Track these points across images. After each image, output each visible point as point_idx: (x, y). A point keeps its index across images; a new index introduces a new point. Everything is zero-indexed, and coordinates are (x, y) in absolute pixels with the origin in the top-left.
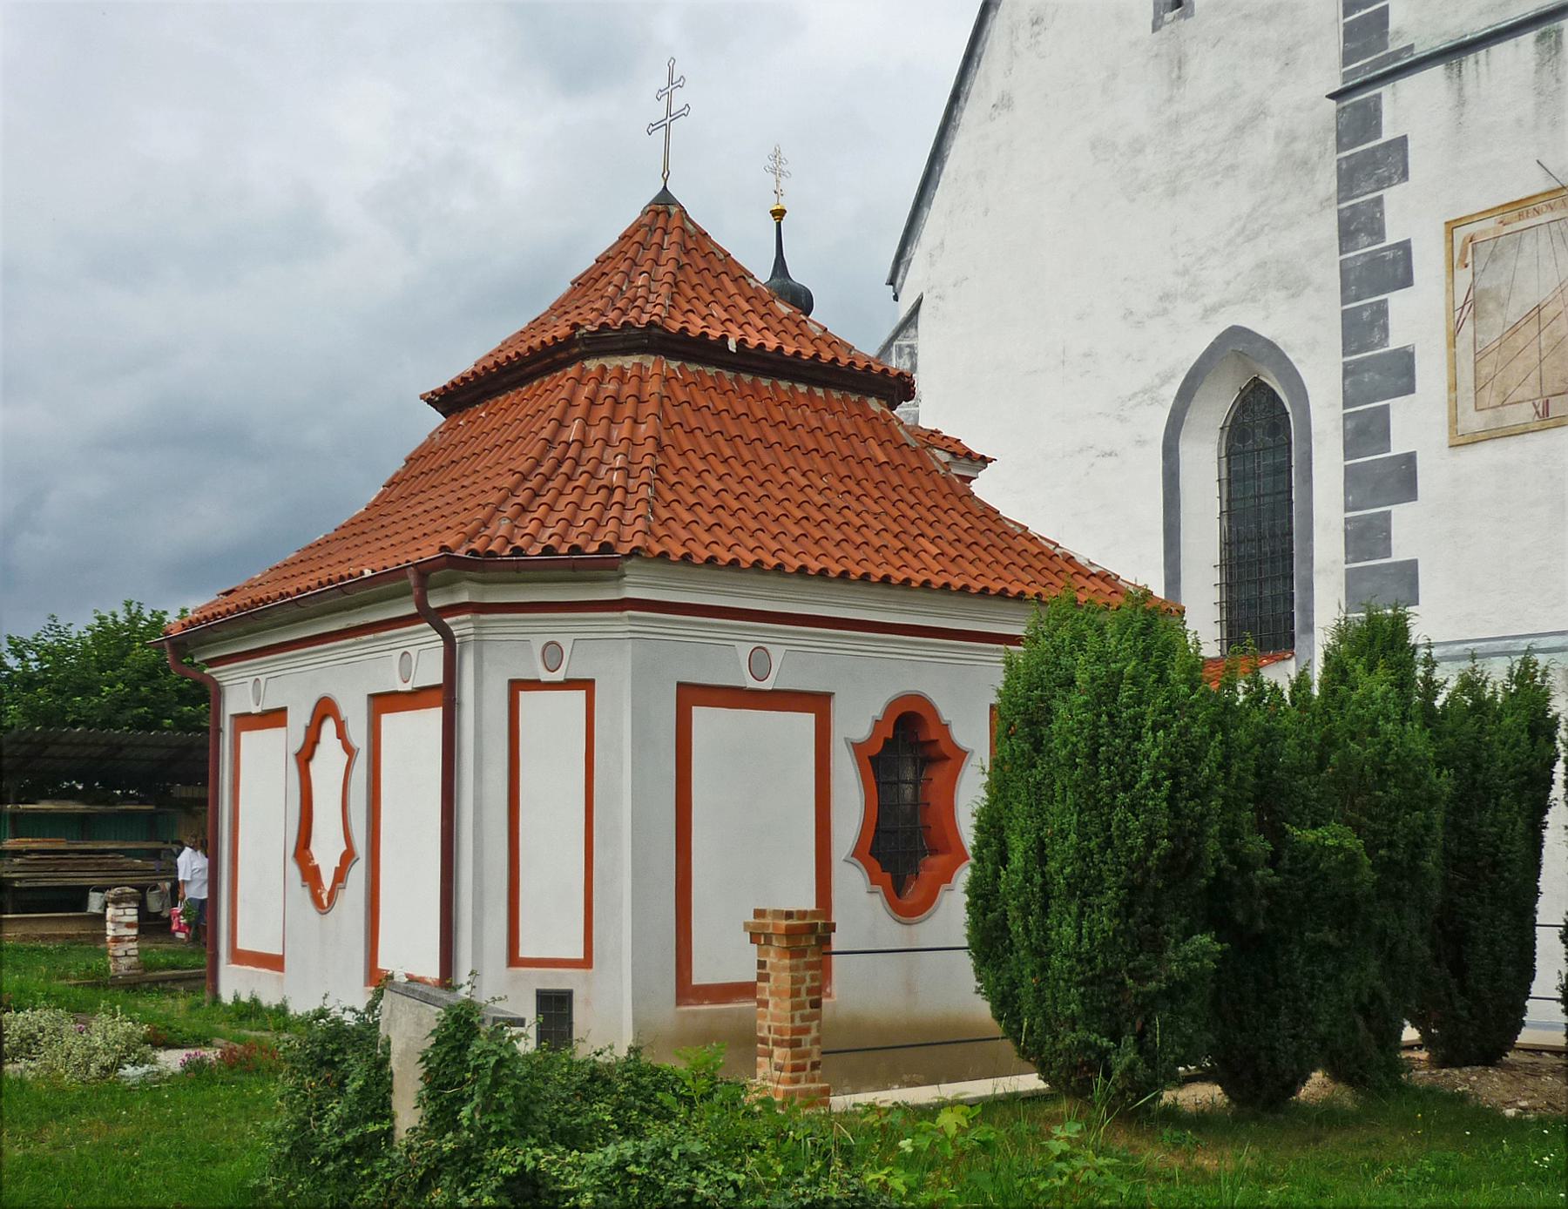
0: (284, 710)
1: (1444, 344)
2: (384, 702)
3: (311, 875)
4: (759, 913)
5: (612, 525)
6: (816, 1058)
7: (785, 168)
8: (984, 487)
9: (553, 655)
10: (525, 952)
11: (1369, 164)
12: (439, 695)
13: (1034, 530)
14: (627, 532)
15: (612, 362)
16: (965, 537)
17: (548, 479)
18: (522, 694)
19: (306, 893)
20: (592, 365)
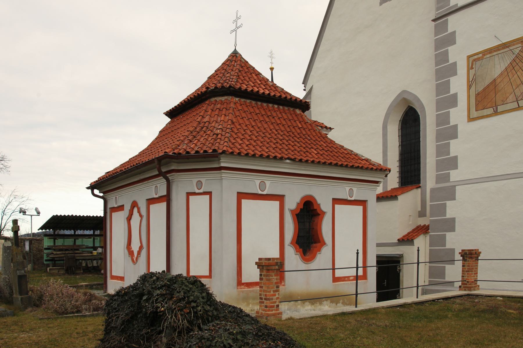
0: (123, 205)
1: (466, 92)
2: (151, 201)
3: (131, 253)
4: (260, 259)
5: (217, 144)
6: (277, 304)
7: (273, 56)
8: (331, 135)
9: (199, 184)
11: (444, 41)
12: (165, 198)
13: (346, 146)
14: (221, 147)
15: (218, 99)
16: (325, 148)
17: (198, 133)
18: (190, 197)
19: (130, 258)
20: (213, 100)
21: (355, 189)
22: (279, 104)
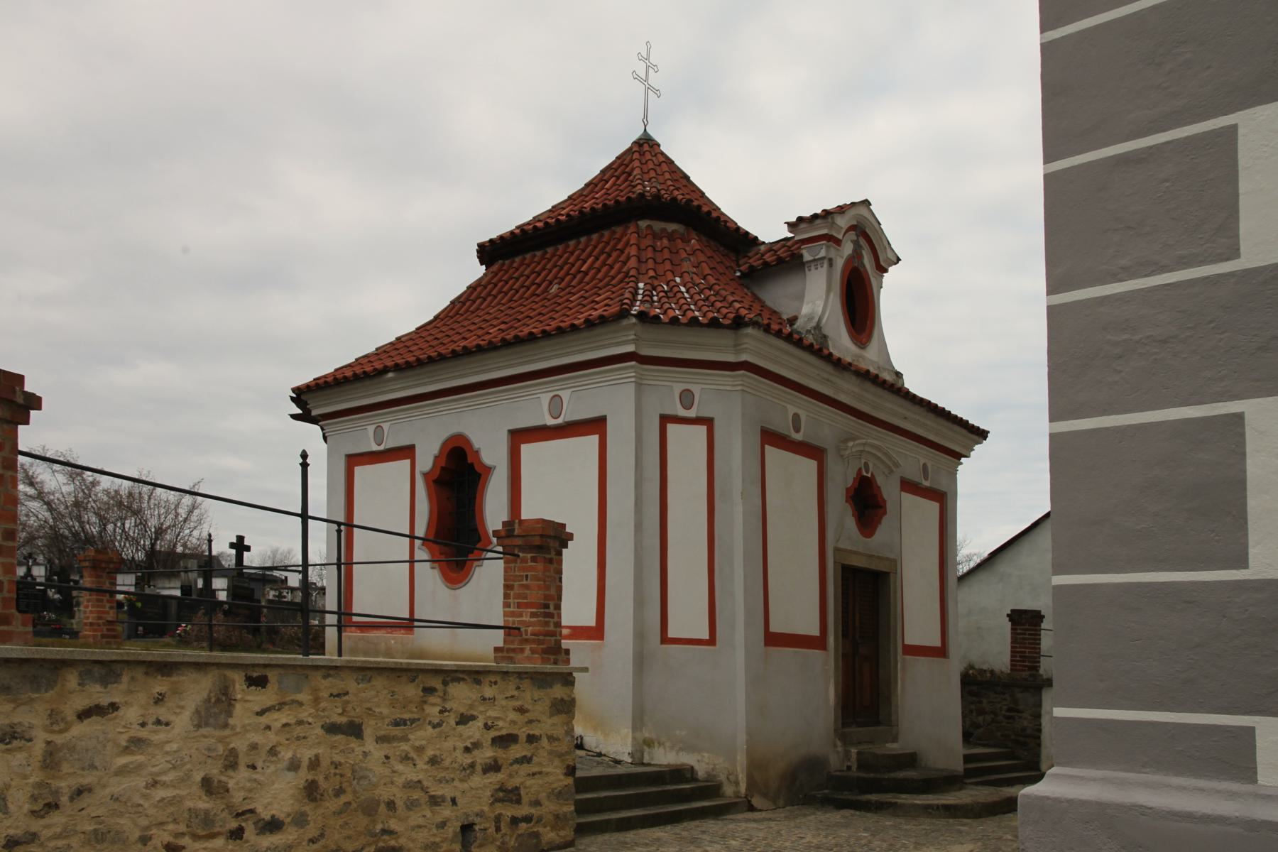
0: (982, 434)
9: (687, 398)
10: (672, 633)
18: (525, 448)
20: (643, 224)
21: (565, 395)
22: (588, 232)
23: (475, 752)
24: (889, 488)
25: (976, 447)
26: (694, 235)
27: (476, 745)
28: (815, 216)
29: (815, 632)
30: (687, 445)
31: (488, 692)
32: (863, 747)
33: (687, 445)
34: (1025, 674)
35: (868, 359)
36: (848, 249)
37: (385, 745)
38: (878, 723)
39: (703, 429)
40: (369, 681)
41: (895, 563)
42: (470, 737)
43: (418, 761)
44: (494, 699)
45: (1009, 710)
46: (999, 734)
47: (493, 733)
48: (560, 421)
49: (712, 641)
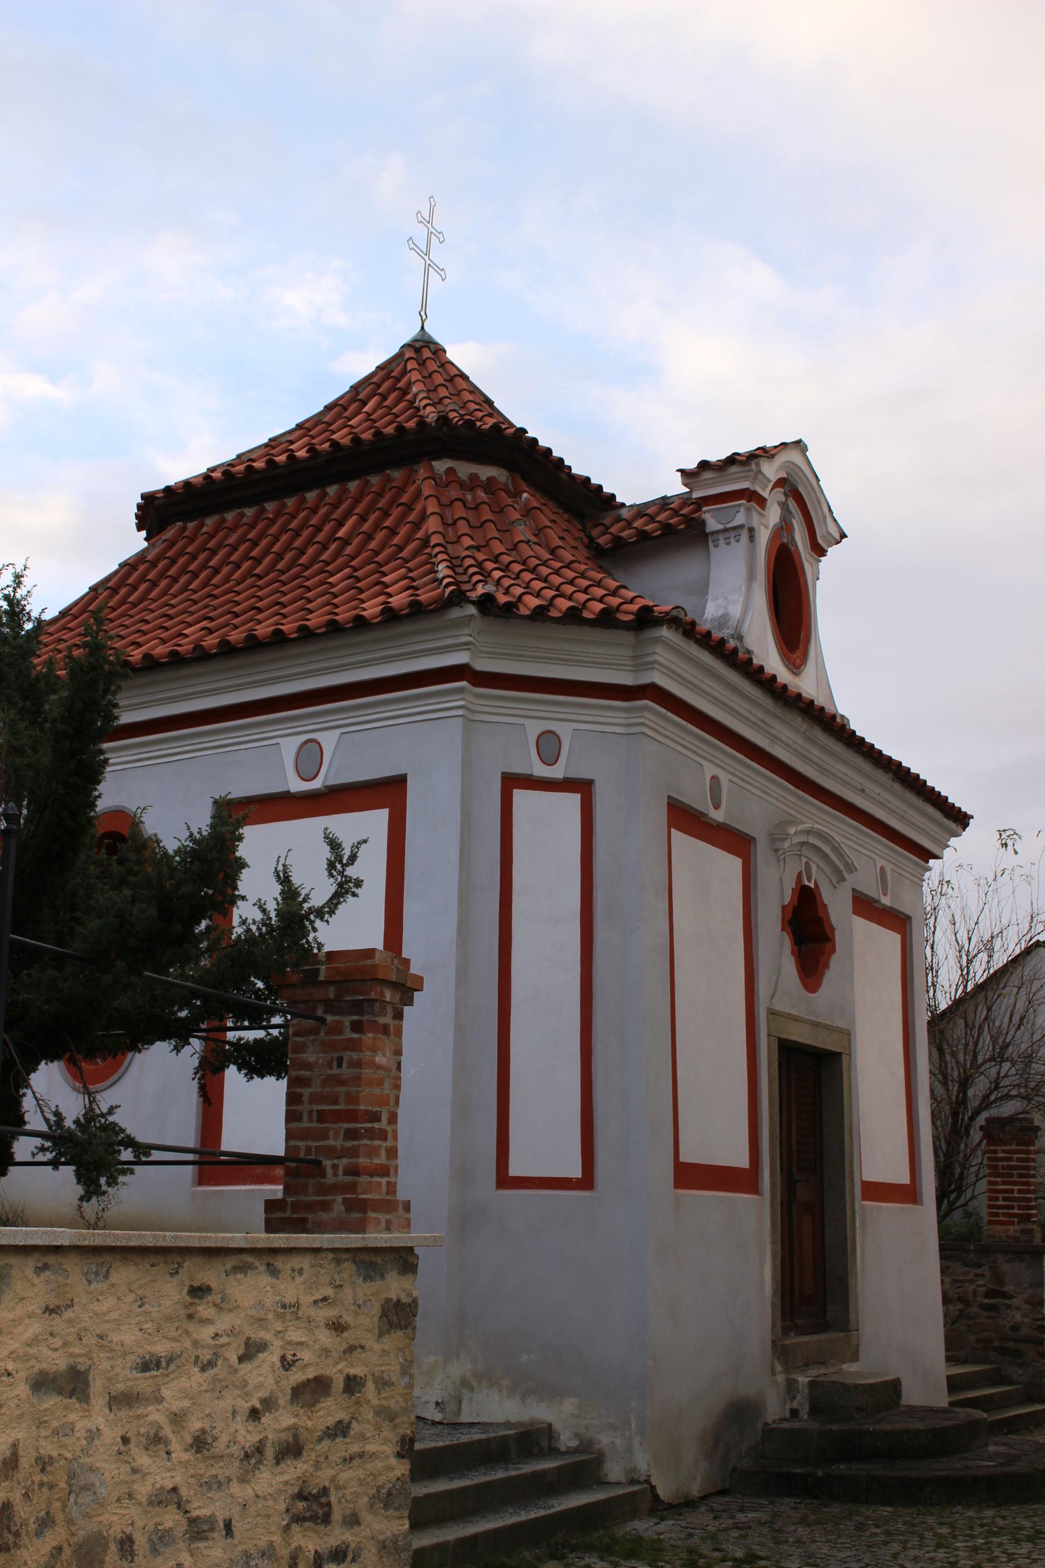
9: (548, 746)
20: (440, 466)
21: (328, 740)
23: (266, 1419)
24: (837, 906)
25: (953, 841)
26: (524, 486)
27: (269, 1404)
28: (732, 460)
29: (743, 1161)
30: (547, 826)
31: (290, 1290)
32: (813, 1372)
33: (547, 826)
34: (1013, 1229)
35: (805, 685)
36: (773, 515)
37: (124, 1413)
38: (824, 1327)
39: (573, 800)
40: (107, 1276)
41: (847, 1035)
42: (260, 1386)
43: (175, 1445)
44: (297, 1305)
45: (989, 1294)
46: (972, 1338)
47: (297, 1376)
48: (317, 784)
49: (586, 1182)
